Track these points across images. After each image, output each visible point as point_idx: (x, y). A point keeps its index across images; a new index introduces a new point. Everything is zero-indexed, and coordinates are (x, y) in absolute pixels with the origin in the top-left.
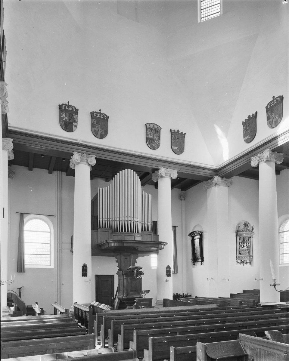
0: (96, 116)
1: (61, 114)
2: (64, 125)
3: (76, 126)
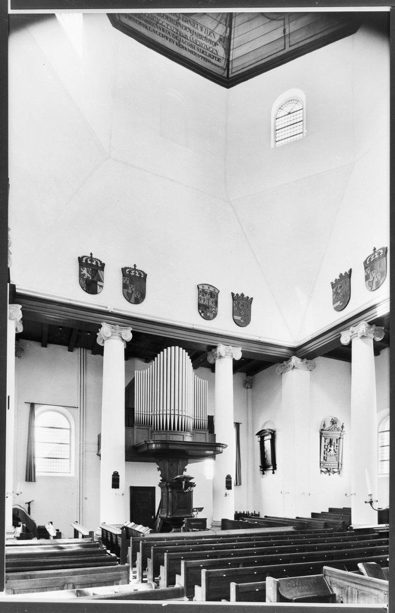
3: (102, 286)
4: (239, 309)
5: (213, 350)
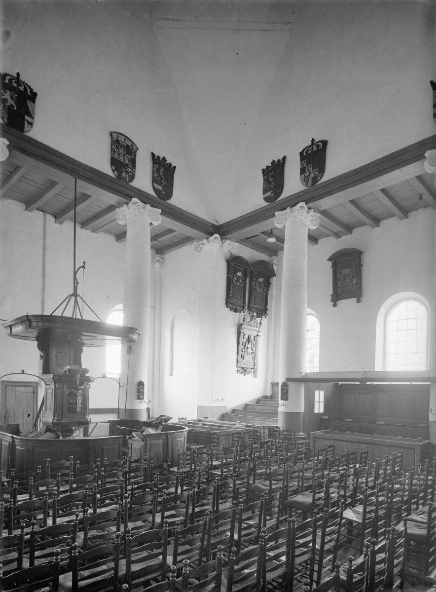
2: (7, 115)
3: (31, 124)
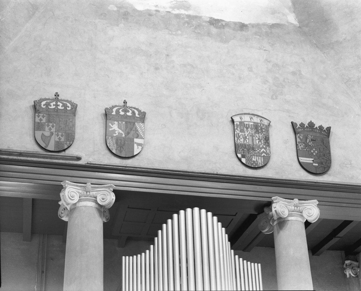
0: (47, 106)
1: (110, 124)
2: (115, 145)
4: (307, 145)
5: (266, 210)
